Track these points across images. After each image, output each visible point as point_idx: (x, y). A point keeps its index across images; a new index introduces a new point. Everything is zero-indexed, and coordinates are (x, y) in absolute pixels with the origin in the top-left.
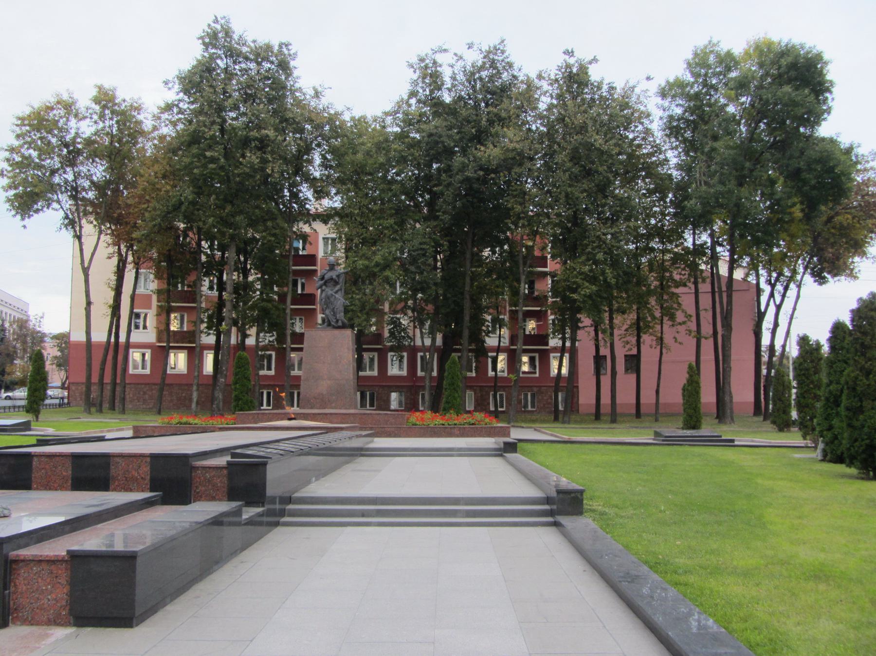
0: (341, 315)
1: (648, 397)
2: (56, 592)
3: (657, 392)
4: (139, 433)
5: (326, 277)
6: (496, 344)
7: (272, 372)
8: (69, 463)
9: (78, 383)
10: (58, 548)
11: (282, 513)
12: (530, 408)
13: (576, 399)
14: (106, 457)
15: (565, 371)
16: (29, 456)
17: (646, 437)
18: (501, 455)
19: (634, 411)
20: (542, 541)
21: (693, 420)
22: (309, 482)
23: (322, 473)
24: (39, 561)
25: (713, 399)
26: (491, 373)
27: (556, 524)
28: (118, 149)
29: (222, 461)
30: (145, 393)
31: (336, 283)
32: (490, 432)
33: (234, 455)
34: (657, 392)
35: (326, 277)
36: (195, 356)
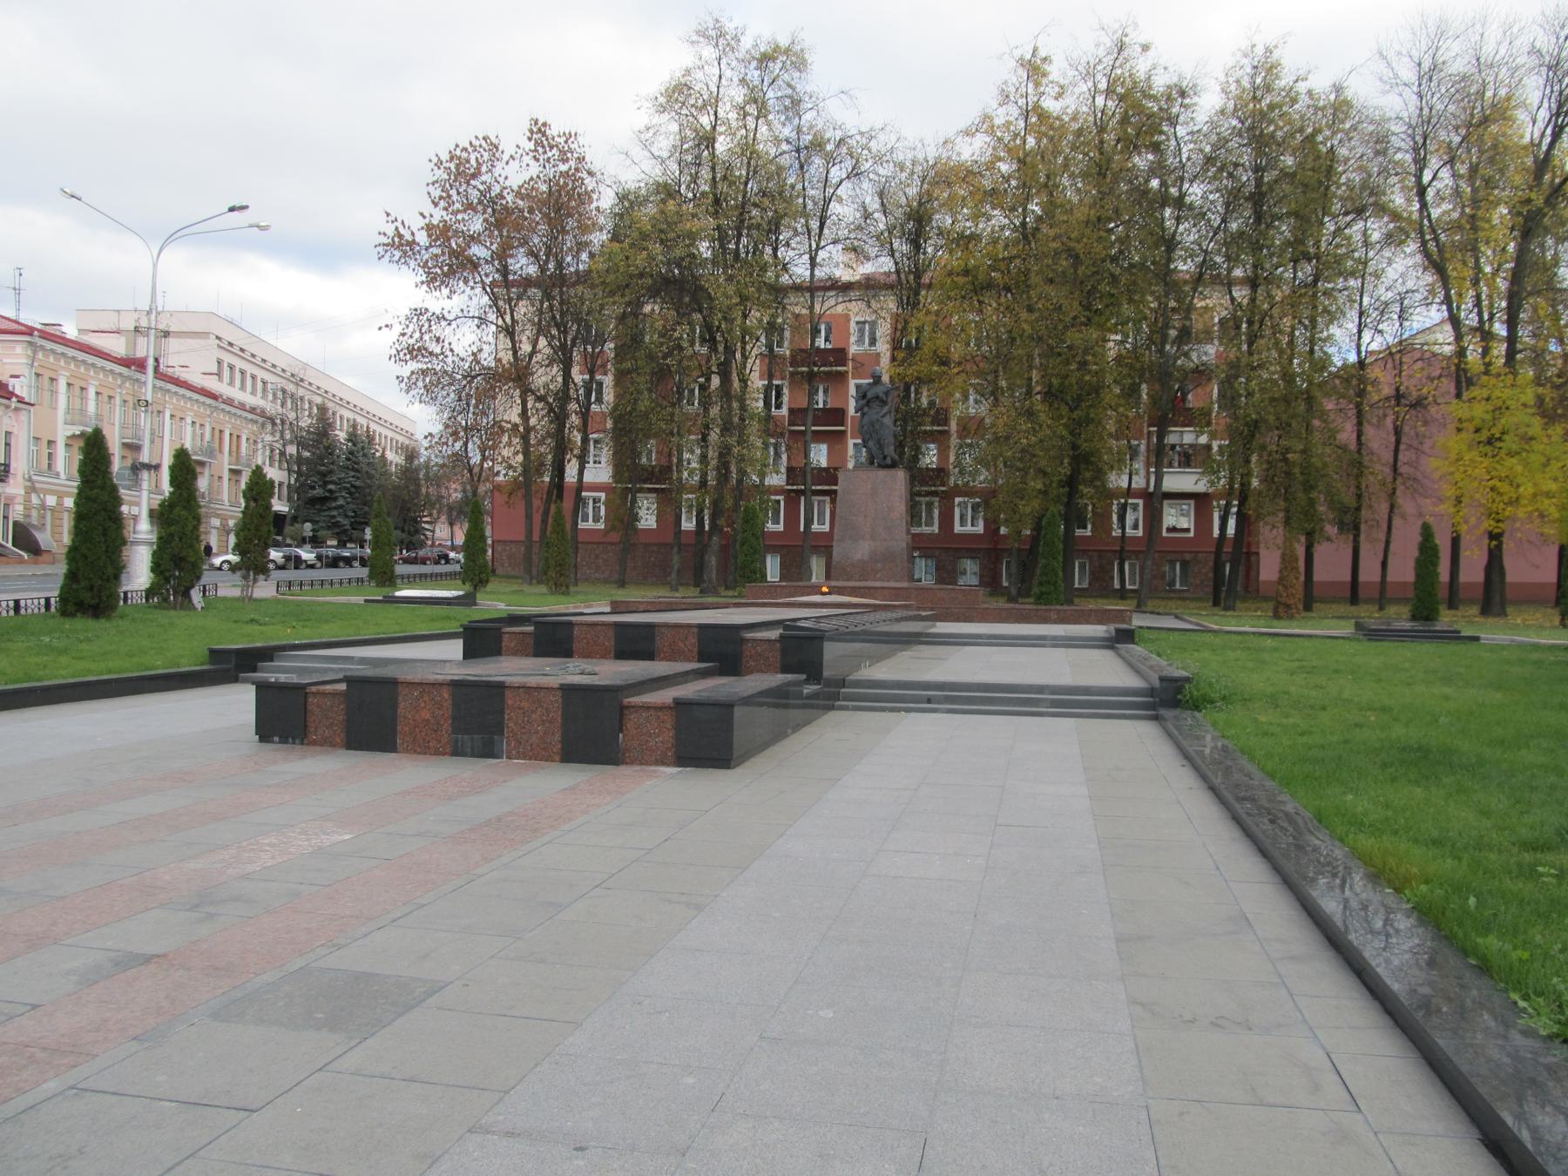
0: (890, 450)
1: (1369, 572)
2: (665, 736)
3: (1384, 564)
4: (617, 608)
5: (869, 395)
6: (1125, 485)
7: (781, 527)
8: (611, 633)
9: (505, 542)
10: (666, 696)
11: (836, 697)
12: (1178, 586)
13: (1253, 573)
14: (650, 626)
15: (1231, 530)
16: (571, 624)
17: (1346, 629)
18: (1111, 647)
19: (1348, 594)
20: (1140, 742)
21: (1424, 611)
22: (858, 667)
23: (876, 659)
24: (647, 707)
25: (1479, 577)
26: (1117, 533)
27: (1156, 718)
28: (561, 202)
29: (774, 634)
30: (597, 557)
31: (884, 403)
32: (1101, 617)
33: (786, 628)
34: (1384, 564)
35: (869, 395)
36: (669, 502)
